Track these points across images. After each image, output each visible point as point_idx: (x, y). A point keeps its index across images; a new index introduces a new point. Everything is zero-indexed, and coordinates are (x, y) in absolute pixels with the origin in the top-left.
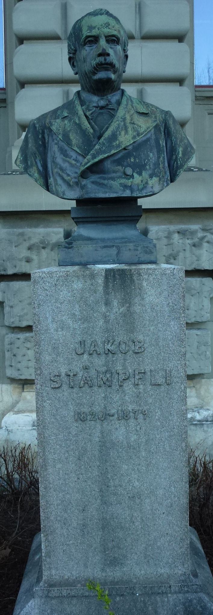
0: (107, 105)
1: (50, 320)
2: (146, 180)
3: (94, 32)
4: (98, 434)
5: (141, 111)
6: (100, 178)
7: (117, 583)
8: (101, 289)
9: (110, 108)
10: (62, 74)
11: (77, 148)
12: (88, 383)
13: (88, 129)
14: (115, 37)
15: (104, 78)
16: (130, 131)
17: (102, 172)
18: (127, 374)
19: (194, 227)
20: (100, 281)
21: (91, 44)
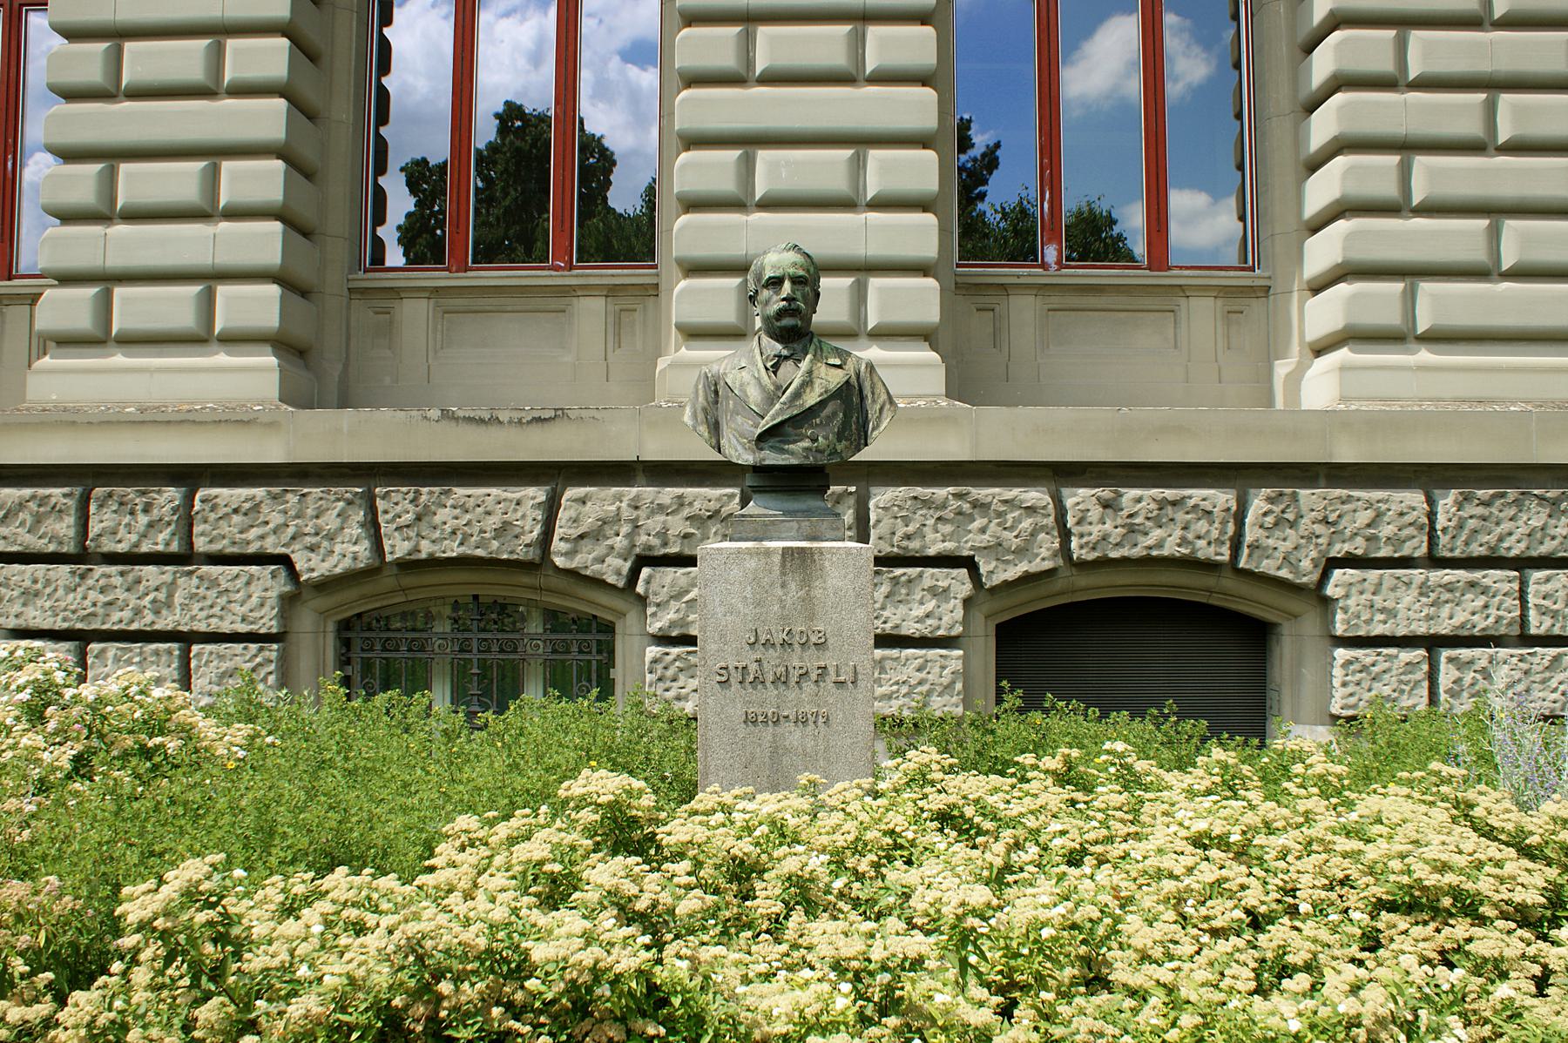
1: (717, 603)
4: (769, 738)
6: (780, 441)
8: (777, 569)
12: (758, 681)
18: (586, 887)
19: (942, 492)
20: (777, 559)
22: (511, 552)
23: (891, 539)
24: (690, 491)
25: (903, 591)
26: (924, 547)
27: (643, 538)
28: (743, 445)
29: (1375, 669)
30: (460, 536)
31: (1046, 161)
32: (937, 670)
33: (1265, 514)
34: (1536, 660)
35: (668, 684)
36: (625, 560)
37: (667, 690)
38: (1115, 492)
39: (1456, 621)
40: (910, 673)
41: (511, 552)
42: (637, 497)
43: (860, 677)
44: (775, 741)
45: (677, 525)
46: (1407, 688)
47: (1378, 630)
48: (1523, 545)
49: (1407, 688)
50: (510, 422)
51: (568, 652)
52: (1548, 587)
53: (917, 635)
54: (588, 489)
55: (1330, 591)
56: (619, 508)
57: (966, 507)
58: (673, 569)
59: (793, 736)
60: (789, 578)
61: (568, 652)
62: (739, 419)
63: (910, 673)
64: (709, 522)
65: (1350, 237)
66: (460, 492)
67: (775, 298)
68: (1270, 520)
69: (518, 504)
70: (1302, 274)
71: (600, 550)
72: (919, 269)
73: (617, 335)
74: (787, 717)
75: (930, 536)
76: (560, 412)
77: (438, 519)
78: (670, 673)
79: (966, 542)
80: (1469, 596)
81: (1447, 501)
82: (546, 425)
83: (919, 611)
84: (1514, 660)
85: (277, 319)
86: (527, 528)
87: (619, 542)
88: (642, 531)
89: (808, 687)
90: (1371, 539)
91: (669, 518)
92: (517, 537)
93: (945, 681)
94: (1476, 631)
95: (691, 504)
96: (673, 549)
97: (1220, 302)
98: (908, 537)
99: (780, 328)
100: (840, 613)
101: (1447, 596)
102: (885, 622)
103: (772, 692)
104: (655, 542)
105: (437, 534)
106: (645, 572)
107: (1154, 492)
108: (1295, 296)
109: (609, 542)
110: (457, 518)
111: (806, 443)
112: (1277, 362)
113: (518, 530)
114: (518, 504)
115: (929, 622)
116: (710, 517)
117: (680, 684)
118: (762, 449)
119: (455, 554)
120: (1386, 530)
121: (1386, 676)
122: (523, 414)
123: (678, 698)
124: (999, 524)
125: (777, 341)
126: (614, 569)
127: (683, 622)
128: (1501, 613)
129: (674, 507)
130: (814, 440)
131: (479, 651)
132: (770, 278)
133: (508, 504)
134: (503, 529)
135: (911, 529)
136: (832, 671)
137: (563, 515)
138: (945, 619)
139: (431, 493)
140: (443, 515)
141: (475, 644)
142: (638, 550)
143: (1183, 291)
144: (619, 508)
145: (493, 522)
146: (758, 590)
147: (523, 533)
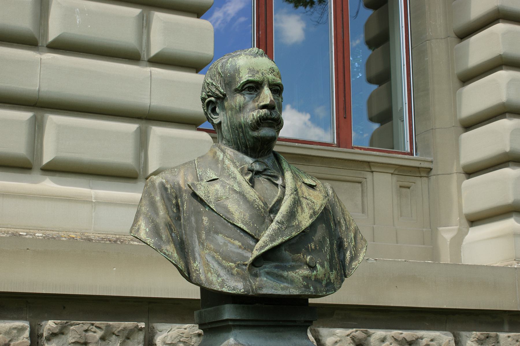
0: (265, 170)
2: (328, 274)
3: (257, 77)
5: (307, 183)
6: (277, 267)
9: (269, 174)
10: (39, 93)
11: (243, 224)
13: (257, 201)
14: (279, 86)
15: (268, 137)
16: (306, 209)
21: (251, 92)
28: (229, 271)
38: (366, 333)
62: (220, 239)
67: (251, 105)
97: (395, 178)
99: (254, 137)
107: (395, 332)
108: (455, 177)
111: (305, 271)
112: (440, 229)
118: (256, 275)
125: (246, 154)
130: (312, 268)
132: (248, 82)
143: (370, 167)
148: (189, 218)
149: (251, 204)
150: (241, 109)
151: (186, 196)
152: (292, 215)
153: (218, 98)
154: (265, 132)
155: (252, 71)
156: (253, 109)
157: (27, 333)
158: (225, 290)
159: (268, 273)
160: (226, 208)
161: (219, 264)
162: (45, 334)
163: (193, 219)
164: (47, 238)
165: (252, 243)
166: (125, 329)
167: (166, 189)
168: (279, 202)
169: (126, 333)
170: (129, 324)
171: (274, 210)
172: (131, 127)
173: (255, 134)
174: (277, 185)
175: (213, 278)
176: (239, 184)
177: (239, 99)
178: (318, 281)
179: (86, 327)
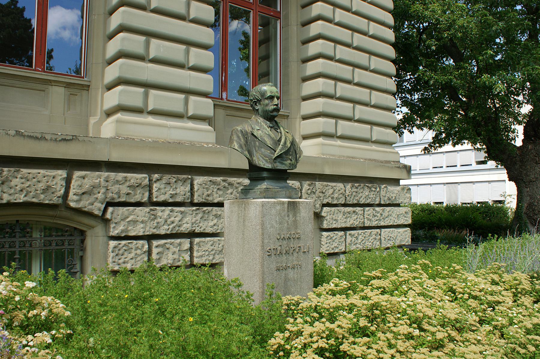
1: (268, 223)
3: (273, 95)
6: (281, 160)
7: (425, 125)
17: (282, 157)
19: (219, 179)
20: (286, 206)
22: (50, 200)
23: (203, 196)
24: (129, 175)
25: (206, 216)
26: (213, 199)
27: (111, 195)
28: (266, 161)
29: (334, 238)
30: (25, 192)
31: (224, 62)
32: (217, 245)
33: (308, 190)
34: (366, 233)
35: (120, 257)
36: (102, 204)
37: (119, 259)
39: (351, 223)
40: (208, 247)
41: (50, 200)
42: (108, 177)
43: (310, 249)
44: (285, 277)
45: (124, 189)
46: (340, 244)
47: (334, 226)
48: (364, 200)
49: (340, 244)
50: (51, 140)
51: (50, 245)
52: (369, 212)
53: (211, 233)
54: (86, 172)
55: (323, 214)
56: (100, 181)
57: (227, 184)
58: (122, 208)
59: (291, 274)
60: (290, 213)
61: (63, 245)
63: (208, 247)
64: (137, 188)
65: (324, 104)
66: (25, 171)
67: (271, 104)
68: (309, 191)
69: (54, 178)
70: (300, 113)
71: (92, 199)
72: (205, 95)
73: (69, 105)
74: (289, 267)
75: (215, 195)
76: (74, 137)
77: (13, 184)
78: (121, 252)
79: (226, 198)
80: (353, 215)
81: (349, 186)
82: (68, 142)
83: (211, 223)
84: (363, 234)
85: (213, 89)
86: (58, 189)
87: (100, 196)
88: (109, 192)
89: (295, 254)
90: (332, 198)
91: (121, 186)
92: (53, 193)
93: (220, 249)
94: (355, 226)
95: (130, 180)
96: (123, 199)
98: (208, 196)
100: (304, 226)
101: (349, 215)
102: (200, 228)
103: (284, 257)
104: (115, 196)
105: (12, 191)
106: (110, 209)
108: (298, 120)
109: (96, 196)
110: (23, 183)
113: (54, 190)
114: (54, 178)
115: (215, 227)
116: (137, 186)
117: (125, 256)
118: (275, 163)
119: (21, 201)
120: (336, 195)
121: (336, 240)
122: (57, 137)
123: (124, 263)
124: (236, 191)
126: (97, 208)
127: (126, 230)
128: (360, 220)
129: (123, 182)
130: (291, 160)
131: (20, 247)
132: (270, 96)
133: (49, 178)
134: (47, 190)
135: (209, 192)
136: (302, 247)
137: (73, 183)
138: (220, 226)
139: (9, 171)
140: (15, 182)
141: (17, 244)
142: (108, 200)
144: (100, 181)
145: (41, 186)
146: (281, 218)
147: (56, 191)
148: (251, 142)
149: (272, 139)
150: (267, 105)
151: (249, 135)
152: (285, 143)
153: (258, 100)
154: (275, 113)
155: (271, 92)
156: (271, 106)
157: (148, 179)
158: (265, 167)
159: (279, 162)
160: (264, 139)
161: (263, 158)
162: (154, 180)
163: (252, 143)
164: (154, 142)
165: (274, 152)
166: (184, 178)
167: (243, 132)
168: (281, 138)
169: (184, 180)
170: (185, 176)
171: (280, 140)
172: (182, 96)
173: (272, 114)
174: (278, 132)
175: (261, 163)
176: (268, 132)
177: (267, 102)
178: (293, 165)
179: (169, 177)
